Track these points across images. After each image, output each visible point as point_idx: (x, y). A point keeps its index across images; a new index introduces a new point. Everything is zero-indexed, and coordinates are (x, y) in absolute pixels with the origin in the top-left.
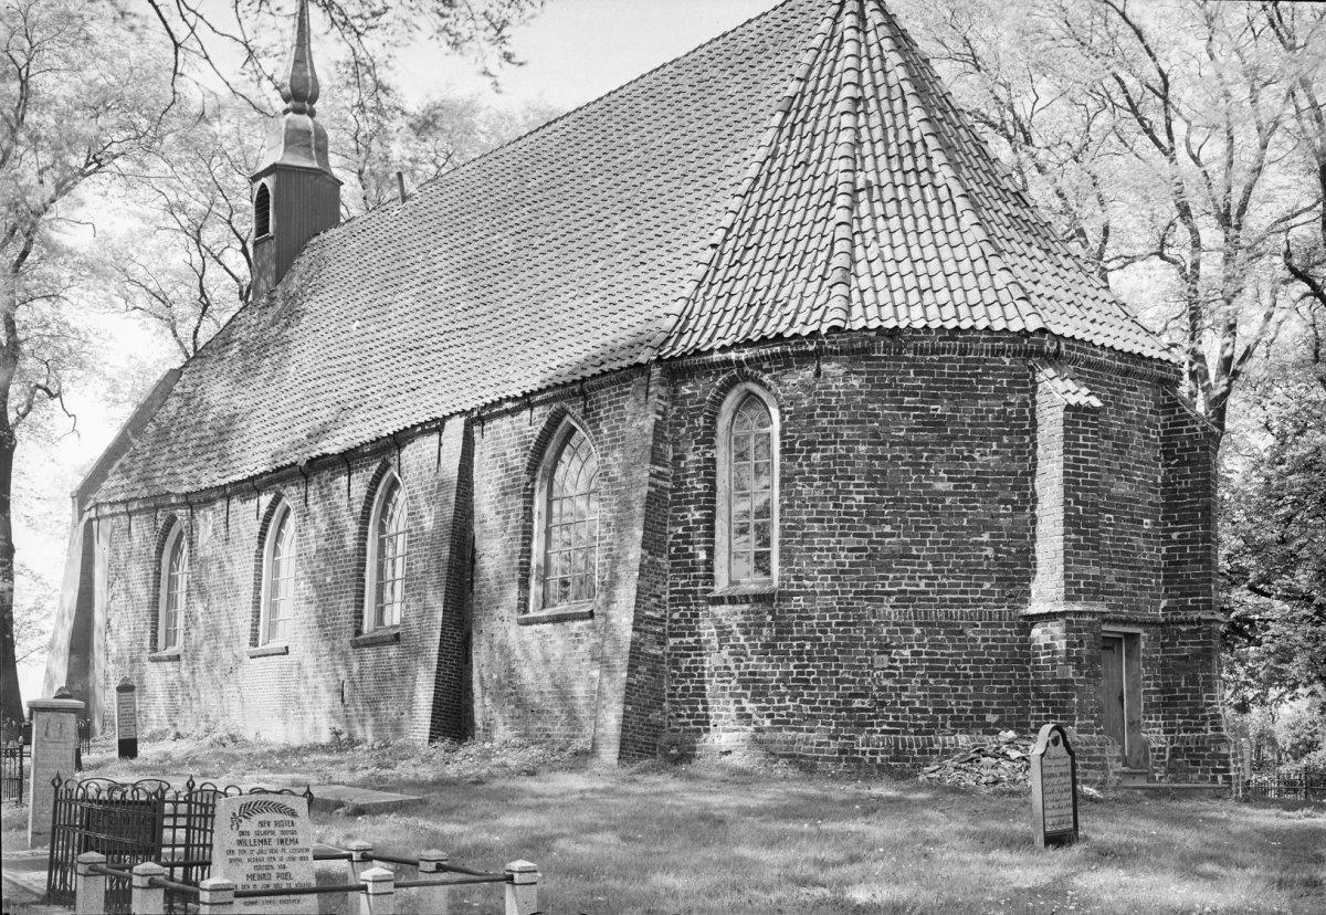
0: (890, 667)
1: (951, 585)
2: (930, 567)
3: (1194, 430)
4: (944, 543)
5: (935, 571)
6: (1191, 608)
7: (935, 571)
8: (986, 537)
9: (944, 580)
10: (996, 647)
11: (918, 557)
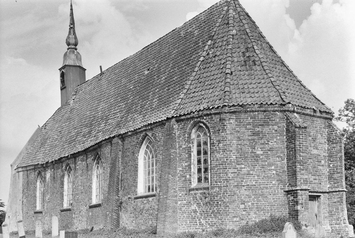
0: (245, 208)
1: (263, 183)
2: (256, 177)
3: (337, 133)
4: (260, 170)
5: (258, 178)
6: (336, 187)
7: (258, 178)
8: (273, 168)
9: (261, 181)
10: (277, 201)
11: (252, 174)
